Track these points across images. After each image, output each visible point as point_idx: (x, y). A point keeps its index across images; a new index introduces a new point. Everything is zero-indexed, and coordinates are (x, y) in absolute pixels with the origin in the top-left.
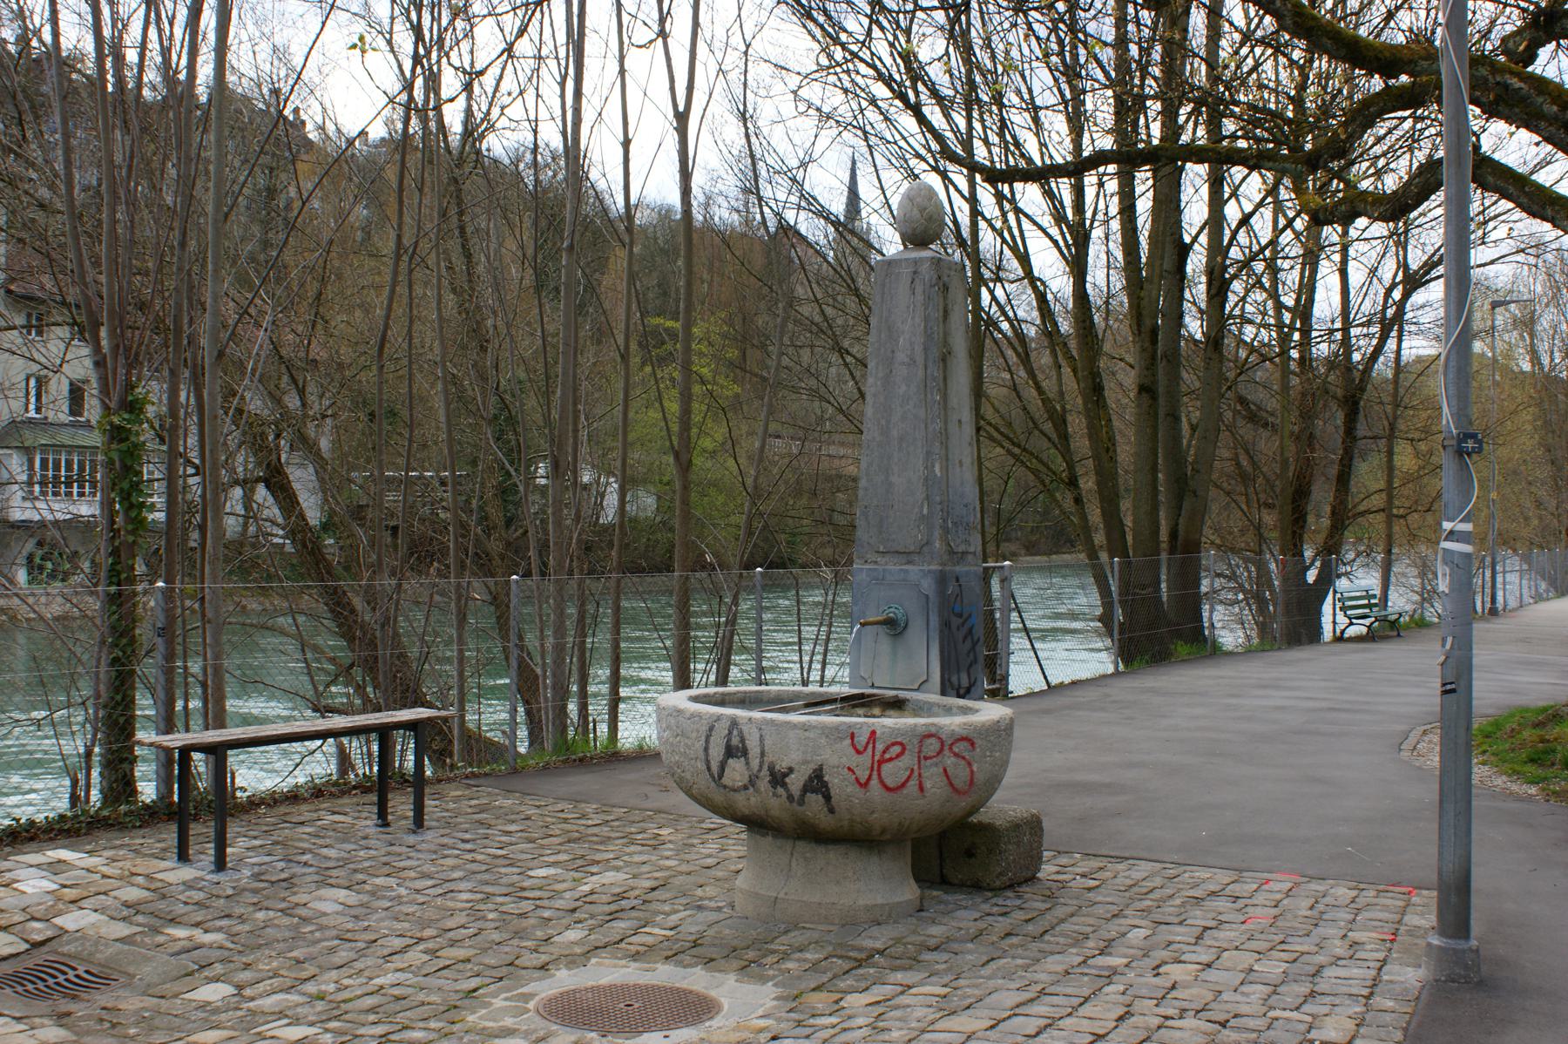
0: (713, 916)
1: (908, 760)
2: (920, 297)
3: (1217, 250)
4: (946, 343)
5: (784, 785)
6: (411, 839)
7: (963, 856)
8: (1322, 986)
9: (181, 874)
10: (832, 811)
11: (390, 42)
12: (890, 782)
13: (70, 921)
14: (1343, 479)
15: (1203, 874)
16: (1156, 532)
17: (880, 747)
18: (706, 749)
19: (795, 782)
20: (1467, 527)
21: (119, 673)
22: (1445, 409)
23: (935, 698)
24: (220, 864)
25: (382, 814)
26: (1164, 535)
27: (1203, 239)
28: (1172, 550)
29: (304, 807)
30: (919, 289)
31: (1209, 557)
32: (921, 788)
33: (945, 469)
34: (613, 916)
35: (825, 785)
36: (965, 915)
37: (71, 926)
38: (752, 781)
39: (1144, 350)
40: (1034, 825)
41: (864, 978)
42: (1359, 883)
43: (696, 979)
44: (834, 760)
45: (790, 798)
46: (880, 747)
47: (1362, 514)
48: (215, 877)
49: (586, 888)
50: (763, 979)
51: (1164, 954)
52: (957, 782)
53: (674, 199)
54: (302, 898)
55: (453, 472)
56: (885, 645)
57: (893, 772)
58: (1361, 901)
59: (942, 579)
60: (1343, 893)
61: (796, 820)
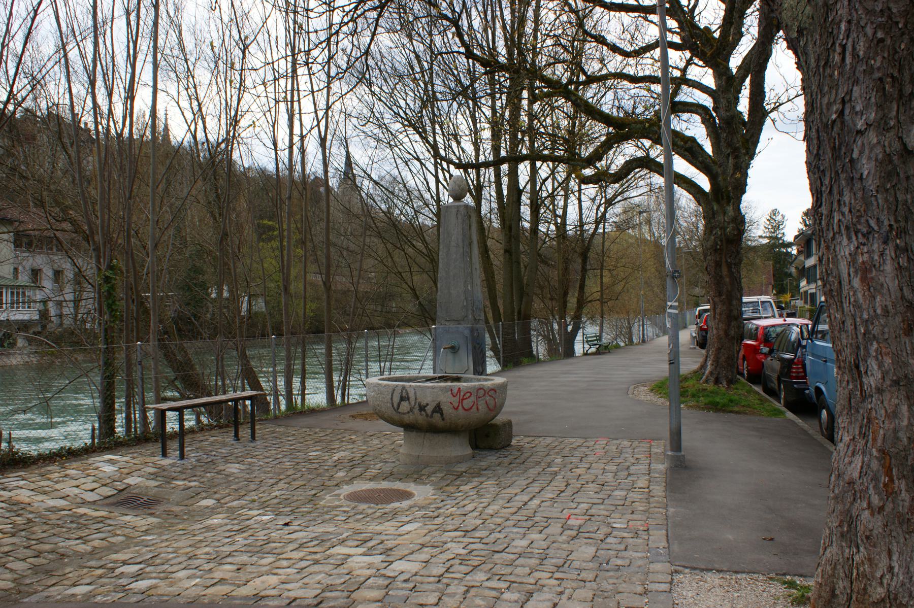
0: (393, 465)
1: (473, 399)
2: (460, 220)
3: (535, 194)
4: (470, 238)
5: (425, 410)
6: (252, 445)
7: (485, 437)
8: (631, 472)
9: (166, 462)
10: (443, 419)
11: (178, 103)
12: (466, 407)
13: (131, 481)
14: (582, 287)
15: (574, 440)
16: (513, 312)
17: (462, 394)
18: (392, 399)
19: (429, 409)
20: (676, 304)
21: (109, 383)
22: (667, 262)
23: (472, 376)
24: (182, 456)
25: (237, 437)
26: (516, 310)
27: (529, 187)
28: (519, 319)
29: (198, 435)
30: (460, 217)
31: (534, 323)
32: (478, 409)
33: (472, 287)
34: (353, 467)
35: (441, 409)
36: (491, 459)
37: (132, 483)
38: (411, 410)
39: (506, 235)
40: (509, 424)
41: (462, 481)
42: (631, 440)
43: (398, 485)
44: (445, 400)
45: (427, 415)
46: (462, 394)
47: (590, 301)
48: (182, 462)
49: (336, 458)
50: (426, 484)
51: (571, 466)
52: (491, 407)
53: (320, 172)
54: (222, 468)
55: (154, 294)
56: (450, 356)
57: (467, 403)
58: (634, 445)
59: (472, 330)
60: (626, 443)
61: (424, 424)
